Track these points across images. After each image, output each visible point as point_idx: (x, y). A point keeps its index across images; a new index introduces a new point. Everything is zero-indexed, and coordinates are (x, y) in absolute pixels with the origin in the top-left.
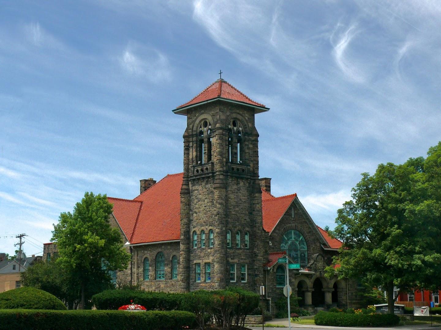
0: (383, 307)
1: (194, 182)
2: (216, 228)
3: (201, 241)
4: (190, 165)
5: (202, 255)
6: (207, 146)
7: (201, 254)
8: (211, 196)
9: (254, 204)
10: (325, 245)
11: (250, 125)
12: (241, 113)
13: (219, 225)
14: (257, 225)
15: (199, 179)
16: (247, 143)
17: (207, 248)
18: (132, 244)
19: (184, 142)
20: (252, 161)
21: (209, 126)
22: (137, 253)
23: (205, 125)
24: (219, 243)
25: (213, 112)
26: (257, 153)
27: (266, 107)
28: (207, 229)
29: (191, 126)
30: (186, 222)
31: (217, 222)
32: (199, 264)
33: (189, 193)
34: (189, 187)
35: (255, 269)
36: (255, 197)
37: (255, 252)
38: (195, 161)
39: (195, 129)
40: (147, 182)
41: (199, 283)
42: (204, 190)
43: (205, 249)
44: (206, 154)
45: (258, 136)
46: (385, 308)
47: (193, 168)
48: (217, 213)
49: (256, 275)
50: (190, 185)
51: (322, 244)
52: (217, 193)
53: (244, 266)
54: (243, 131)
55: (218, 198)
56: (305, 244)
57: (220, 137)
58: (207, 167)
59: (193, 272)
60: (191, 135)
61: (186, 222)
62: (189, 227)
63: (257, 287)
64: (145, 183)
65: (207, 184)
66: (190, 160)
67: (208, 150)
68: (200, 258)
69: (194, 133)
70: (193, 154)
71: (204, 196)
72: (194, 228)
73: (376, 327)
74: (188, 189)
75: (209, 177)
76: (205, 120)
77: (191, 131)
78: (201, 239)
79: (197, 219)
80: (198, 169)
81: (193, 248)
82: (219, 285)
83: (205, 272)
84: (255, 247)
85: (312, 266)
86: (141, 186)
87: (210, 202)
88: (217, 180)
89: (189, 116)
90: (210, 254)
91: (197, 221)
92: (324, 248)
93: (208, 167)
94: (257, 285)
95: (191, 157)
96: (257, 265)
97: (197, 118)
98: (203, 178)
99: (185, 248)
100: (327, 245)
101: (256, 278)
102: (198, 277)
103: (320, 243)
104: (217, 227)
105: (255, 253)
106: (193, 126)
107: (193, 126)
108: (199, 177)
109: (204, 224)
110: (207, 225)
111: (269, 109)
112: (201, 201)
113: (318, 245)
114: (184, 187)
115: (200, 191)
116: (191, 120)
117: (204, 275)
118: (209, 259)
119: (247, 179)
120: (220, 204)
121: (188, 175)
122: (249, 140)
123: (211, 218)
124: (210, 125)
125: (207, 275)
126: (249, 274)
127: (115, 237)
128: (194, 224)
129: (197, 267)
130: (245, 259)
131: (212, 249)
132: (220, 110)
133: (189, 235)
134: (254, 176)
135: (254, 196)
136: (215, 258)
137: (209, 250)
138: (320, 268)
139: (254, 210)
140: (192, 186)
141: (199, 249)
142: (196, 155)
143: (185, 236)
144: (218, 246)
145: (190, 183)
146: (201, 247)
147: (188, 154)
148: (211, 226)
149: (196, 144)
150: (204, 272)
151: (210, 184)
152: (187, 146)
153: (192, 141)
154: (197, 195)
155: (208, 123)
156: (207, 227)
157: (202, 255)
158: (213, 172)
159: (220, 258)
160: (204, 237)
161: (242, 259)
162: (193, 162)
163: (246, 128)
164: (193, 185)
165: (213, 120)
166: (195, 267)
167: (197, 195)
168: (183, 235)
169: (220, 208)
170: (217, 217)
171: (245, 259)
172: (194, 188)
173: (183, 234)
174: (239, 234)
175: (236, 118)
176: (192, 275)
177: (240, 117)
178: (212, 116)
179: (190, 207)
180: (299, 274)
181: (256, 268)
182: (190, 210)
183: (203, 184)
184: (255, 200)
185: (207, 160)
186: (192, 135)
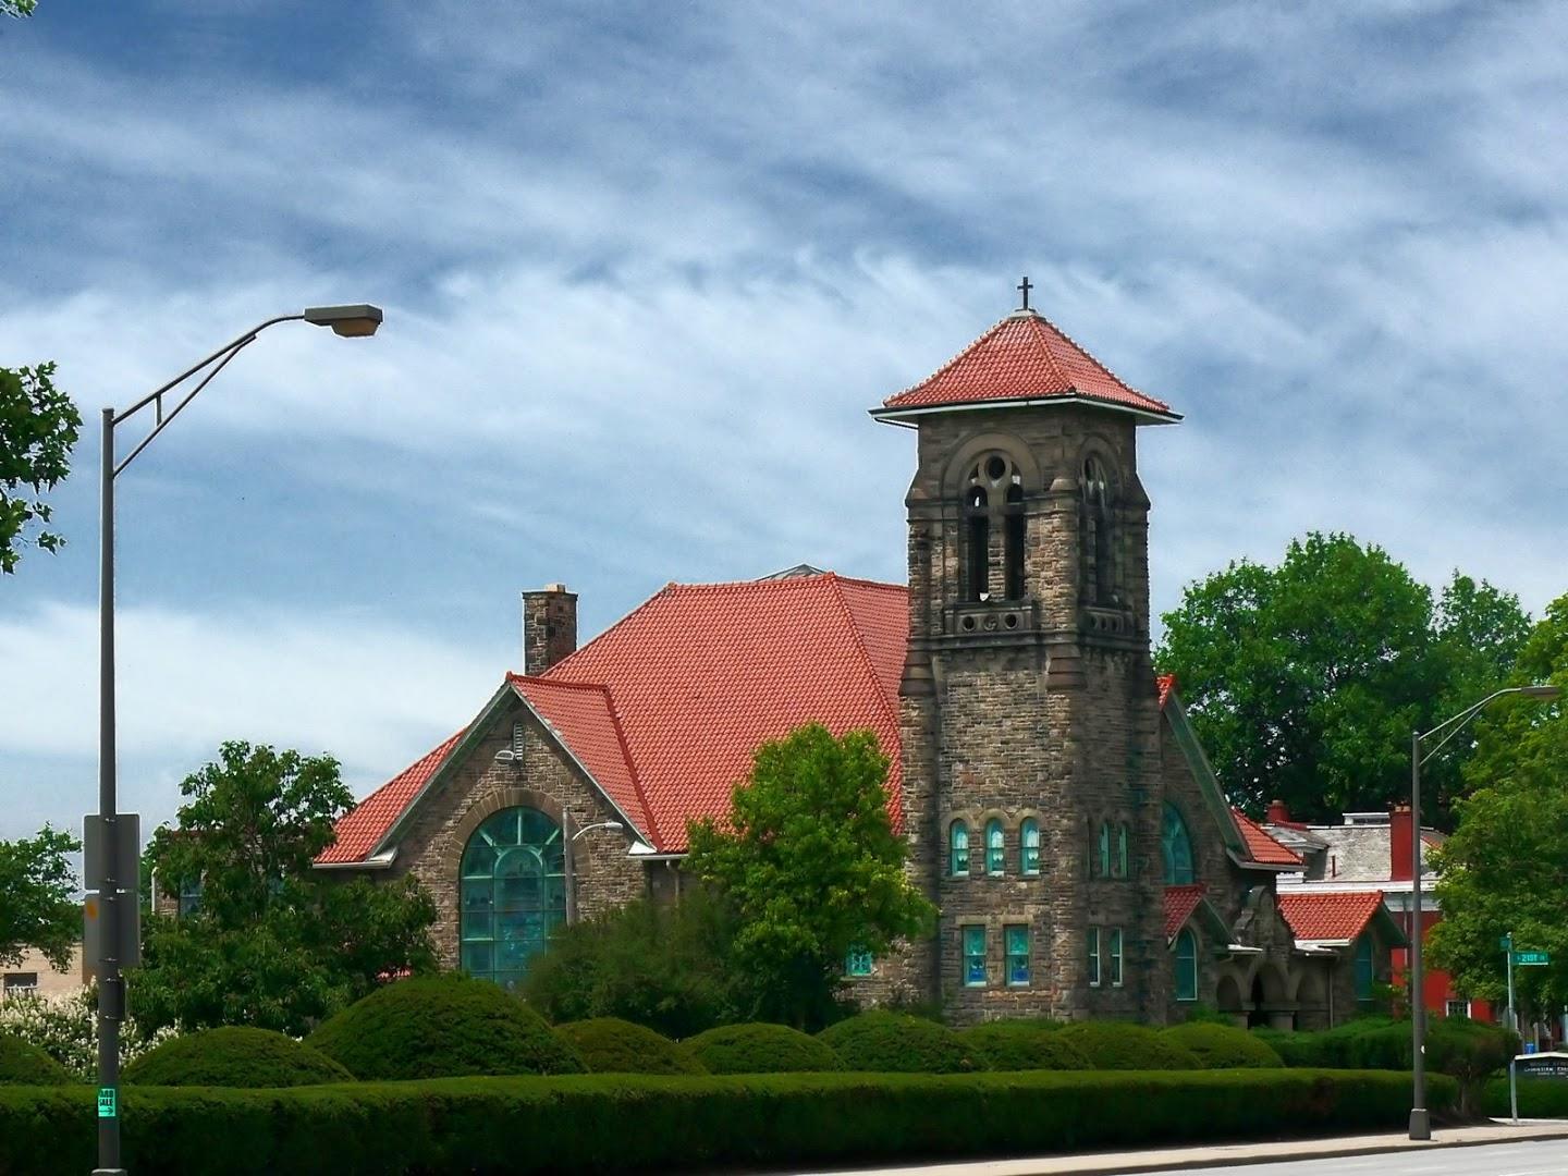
0: (1531, 1064)
1: (953, 658)
2: (1063, 817)
3: (985, 855)
4: (936, 598)
5: (994, 897)
6: (1002, 543)
7: (988, 894)
8: (1029, 710)
9: (1139, 733)
10: (1238, 849)
11: (1126, 472)
12: (1107, 432)
13: (1071, 806)
14: (1151, 801)
15: (975, 650)
16: (1118, 532)
17: (1014, 877)
18: (667, 852)
19: (908, 521)
20: (1131, 591)
21: (1012, 474)
22: (681, 883)
23: (996, 468)
24: (1071, 863)
25: (1035, 435)
26: (1144, 560)
27: (1169, 411)
28: (1011, 815)
29: (936, 468)
30: (927, 788)
31: (1062, 797)
32: (980, 929)
33: (932, 694)
34: (931, 672)
35: (1145, 945)
36: (1145, 710)
37: (1143, 888)
38: (956, 588)
39: (950, 477)
40: (553, 602)
41: (980, 990)
42: (999, 688)
43: (1005, 881)
44: (1001, 567)
45: (1147, 506)
46: (1536, 1067)
47: (952, 612)
48: (1064, 767)
49: (1149, 964)
50: (937, 668)
51: (1231, 849)
52: (1059, 705)
53: (1115, 934)
54: (1108, 492)
55: (1069, 720)
56: (1187, 850)
57: (1069, 521)
58: (1015, 613)
59: (953, 954)
60: (937, 499)
61: (927, 788)
62: (934, 806)
63: (1151, 1001)
64: (548, 604)
65: (1011, 670)
66: (933, 583)
67: (1006, 555)
68: (982, 907)
69: (950, 493)
70: (947, 563)
71: (999, 707)
72: (954, 809)
73: (1261, 1142)
74: (929, 681)
75: (1022, 649)
76: (995, 454)
77: (937, 483)
78: (986, 847)
79: (970, 782)
80: (973, 616)
81: (949, 873)
82: (1072, 998)
83: (1006, 955)
84: (1145, 873)
85: (1248, 929)
86: (528, 617)
87: (1024, 729)
88: (1064, 661)
89: (928, 431)
90: (1027, 896)
91: (971, 787)
92: (1235, 859)
93: (1019, 615)
94: (1152, 996)
95: (936, 572)
96: (1151, 929)
97: (962, 444)
98: (997, 649)
99: (925, 874)
100: (1246, 850)
101: (1147, 972)
102: (971, 969)
103: (1224, 845)
104: (1066, 812)
105: (1142, 894)
106: (945, 470)
107: (945, 470)
108: (999, 643)
109: (998, 798)
110: (1011, 803)
111: (1180, 417)
112: (987, 723)
113: (1219, 849)
114: (916, 672)
115: (985, 691)
116: (933, 449)
117: (1000, 964)
118: (1021, 913)
119: (1125, 652)
120: (1073, 740)
121: (928, 634)
122: (1124, 521)
123: (1030, 781)
124: (1016, 471)
125: (1011, 964)
126: (1128, 961)
127: (456, 808)
128: (959, 796)
129: (966, 935)
130: (1118, 912)
131: (1034, 880)
132: (1063, 429)
133: (938, 833)
134: (1138, 642)
135: (1141, 708)
136: (1059, 912)
137: (1024, 885)
138: (1266, 933)
139: (1140, 754)
140: (944, 672)
141: (979, 879)
142: (959, 569)
143: (922, 836)
144: (1070, 875)
145: (935, 659)
146: (985, 873)
147: (927, 562)
148: (1030, 806)
149: (959, 530)
150: (1000, 954)
151: (1026, 672)
152: (923, 536)
153: (943, 521)
154: (970, 702)
155: (1009, 467)
156: (1013, 810)
157: (994, 897)
158: (1042, 631)
159: (1076, 912)
160: (997, 840)
161: (1113, 912)
162: (946, 589)
163: (1116, 482)
164: (950, 667)
165: (1037, 462)
166: (960, 938)
167: (970, 702)
168: (917, 832)
169: (1072, 754)
170: (1065, 781)
171: (1118, 912)
172: (953, 678)
173: (917, 829)
174: (1106, 832)
175: (1095, 453)
176: (950, 963)
177: (1102, 446)
178: (1029, 445)
179: (936, 741)
180: (1228, 956)
181: (1148, 942)
182: (939, 750)
183: (996, 668)
184: (1143, 719)
185: (1003, 587)
186: (941, 498)
